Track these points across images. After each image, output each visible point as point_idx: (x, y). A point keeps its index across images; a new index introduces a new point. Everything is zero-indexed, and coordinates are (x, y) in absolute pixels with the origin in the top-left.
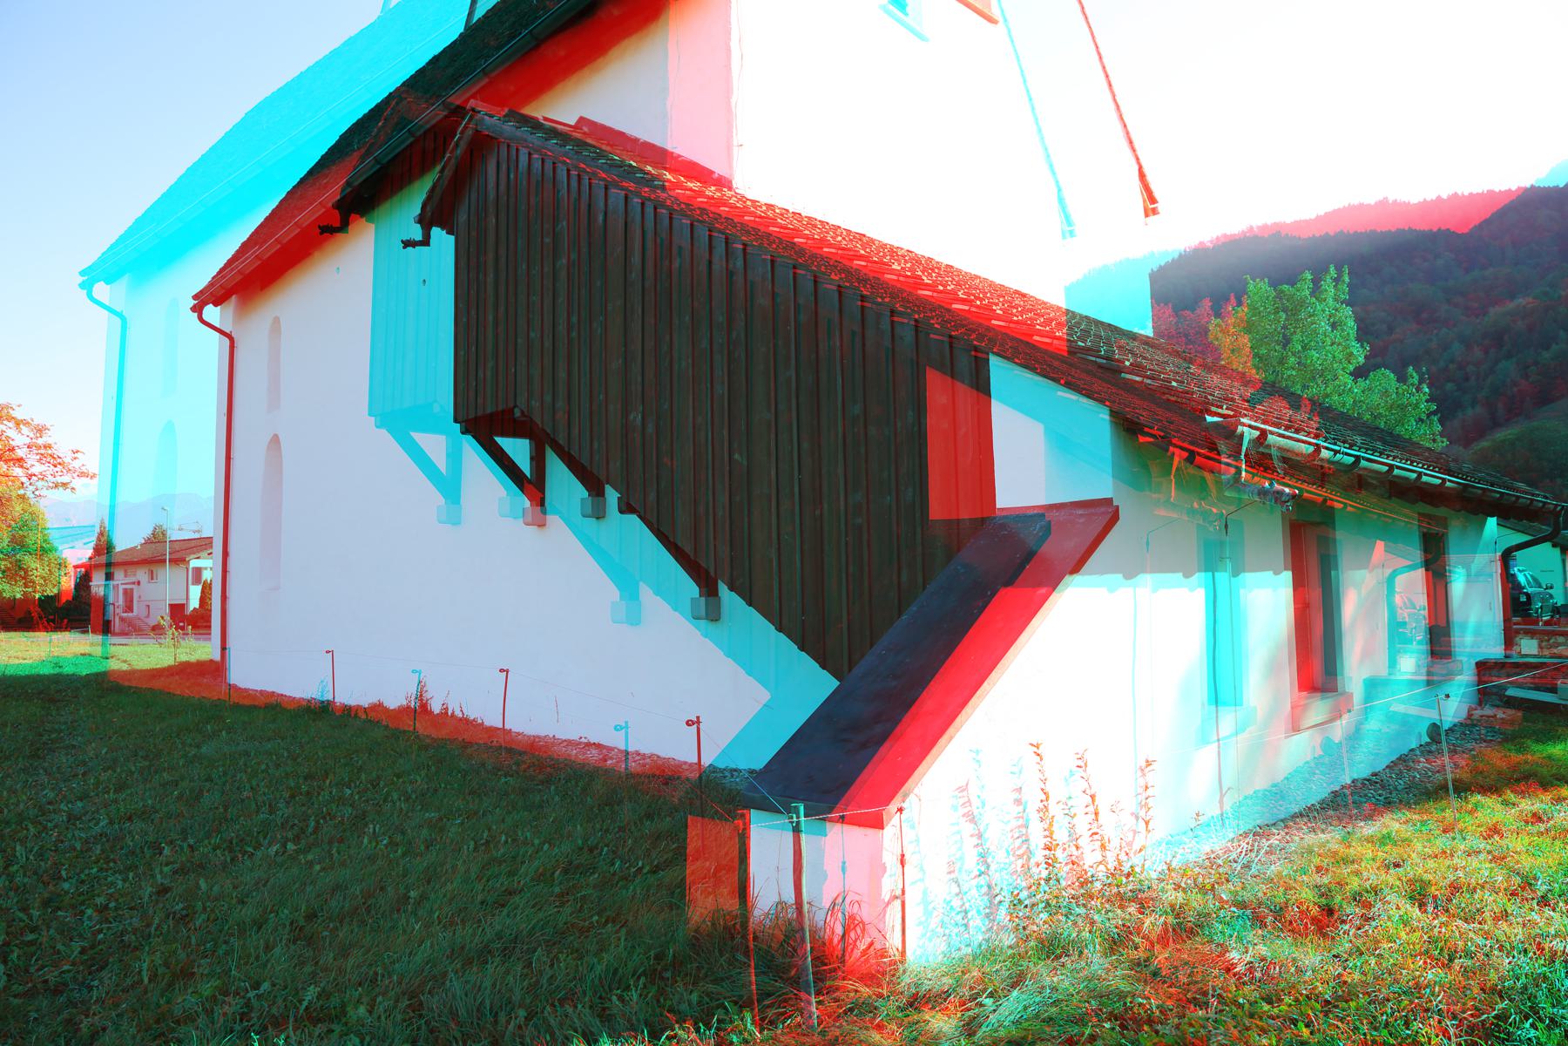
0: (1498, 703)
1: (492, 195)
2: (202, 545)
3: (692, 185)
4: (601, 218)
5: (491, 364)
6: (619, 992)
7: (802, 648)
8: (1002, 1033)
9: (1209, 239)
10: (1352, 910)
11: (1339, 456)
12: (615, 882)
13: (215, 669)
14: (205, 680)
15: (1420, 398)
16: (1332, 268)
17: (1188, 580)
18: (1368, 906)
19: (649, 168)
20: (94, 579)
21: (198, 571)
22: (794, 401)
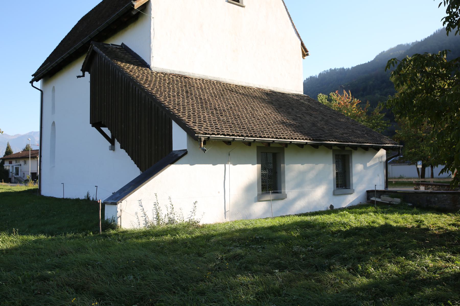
13: (38, 191)
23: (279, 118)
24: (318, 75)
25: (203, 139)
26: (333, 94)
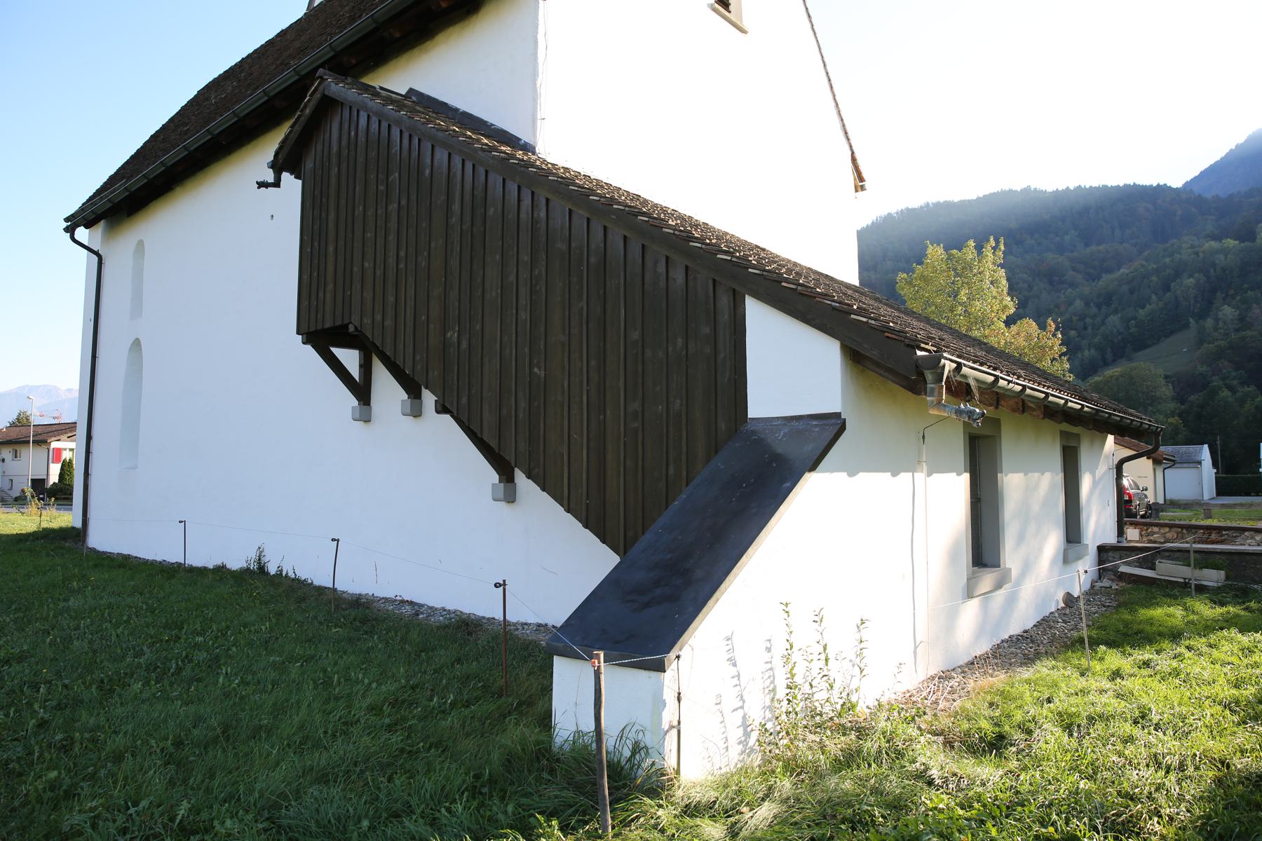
0: (1114, 577)
1: (335, 149)
2: (67, 429)
3: (504, 149)
4: (427, 172)
5: (330, 287)
6: (447, 804)
7: (586, 526)
8: (759, 834)
9: (895, 211)
10: (1017, 736)
11: (1011, 385)
12: (435, 715)
13: (77, 535)
14: (67, 544)
15: (1055, 344)
16: (992, 239)
17: (896, 478)
18: (1029, 732)
19: (469, 133)
21: (58, 452)
22: (585, 327)
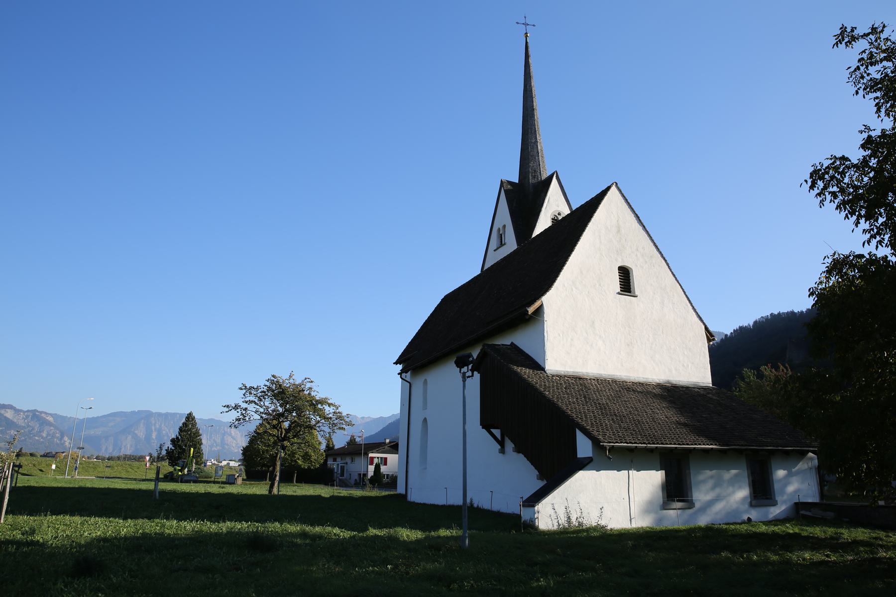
20: (328, 461)
23: (682, 420)
24: (751, 324)
25: (608, 448)
26: (765, 369)
